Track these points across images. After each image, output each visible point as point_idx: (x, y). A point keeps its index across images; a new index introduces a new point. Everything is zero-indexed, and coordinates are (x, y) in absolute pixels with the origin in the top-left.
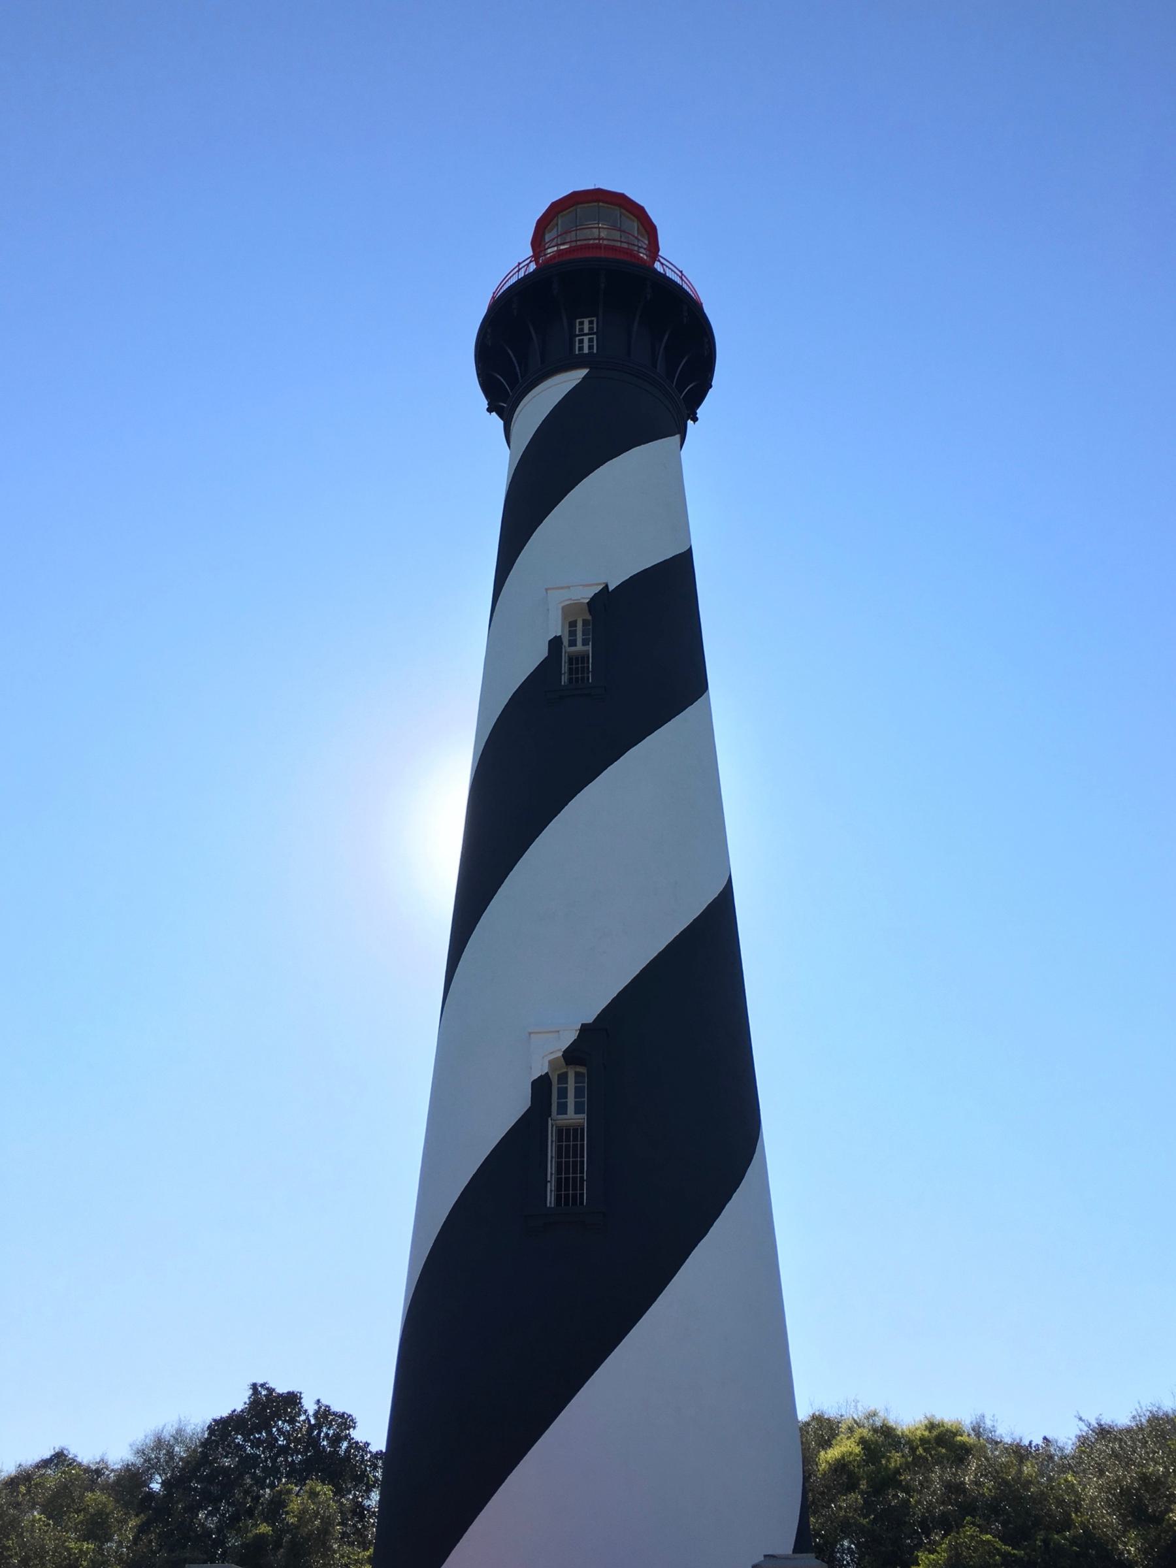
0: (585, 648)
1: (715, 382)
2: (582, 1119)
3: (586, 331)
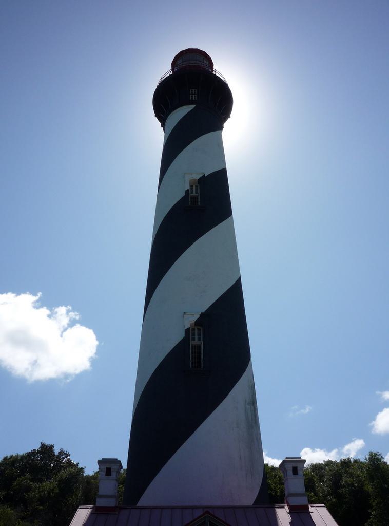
0: (197, 194)
1: (231, 115)
2: (201, 343)
3: (193, 93)
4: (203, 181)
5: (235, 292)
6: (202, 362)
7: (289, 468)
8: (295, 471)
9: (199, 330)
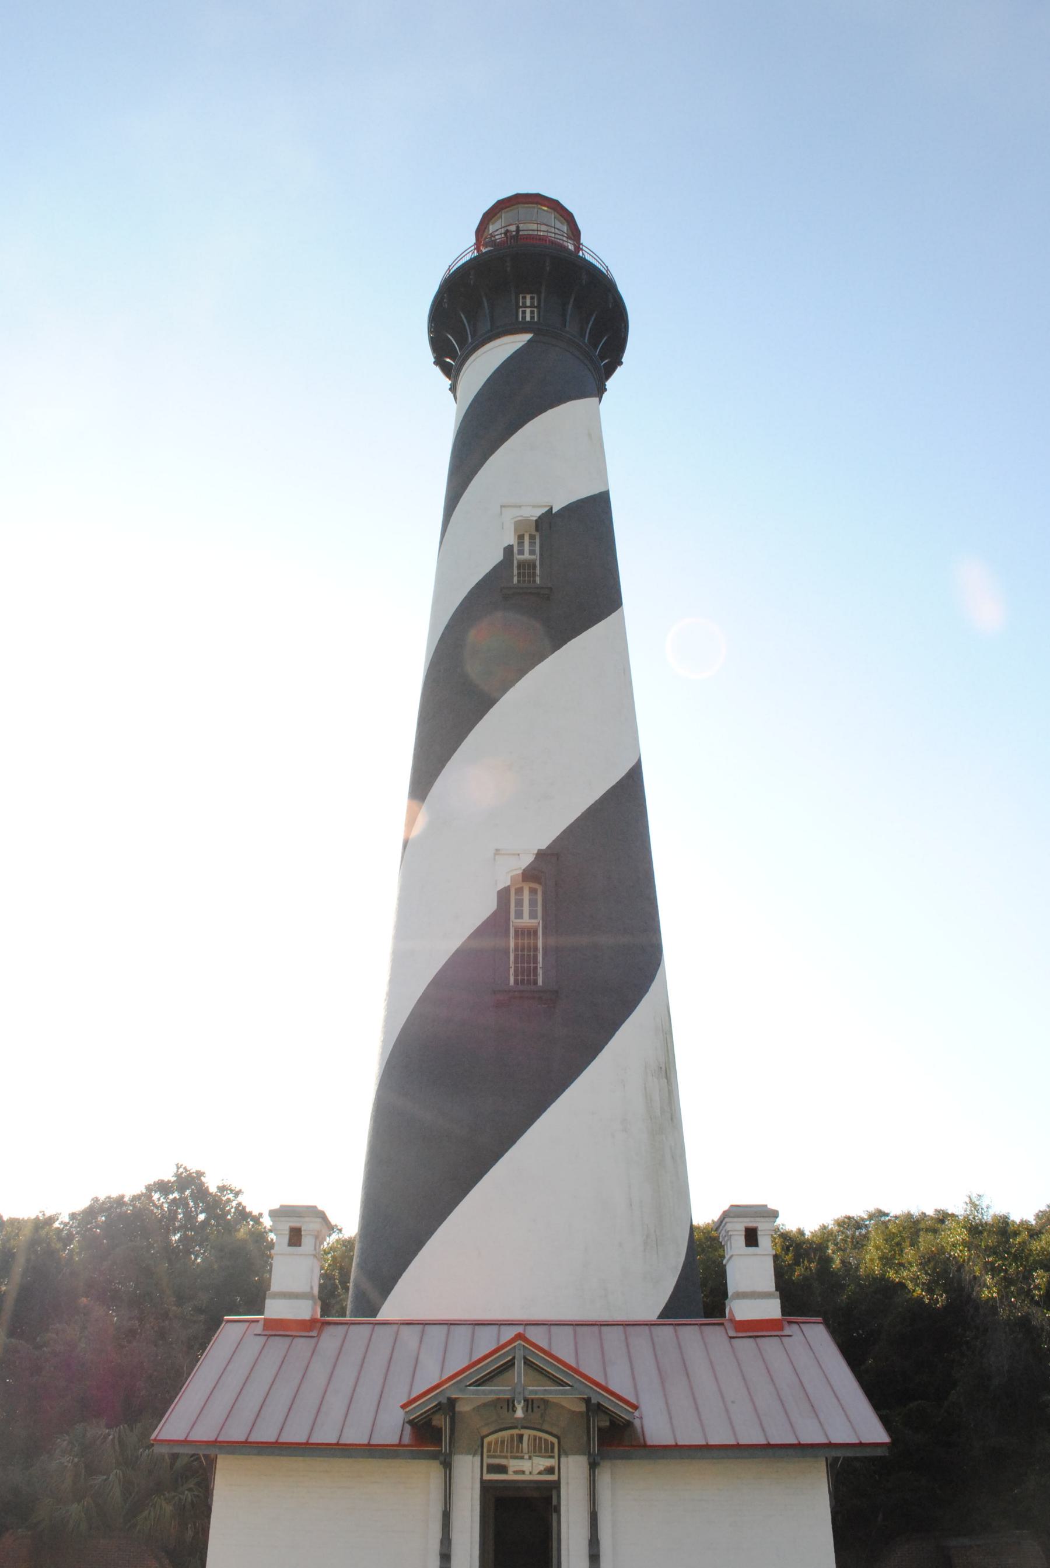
1: (626, 358)
3: (528, 303)
4: (548, 524)
5: (628, 793)
6: (540, 971)
7: (737, 1228)
8: (751, 1237)
9: (533, 891)
